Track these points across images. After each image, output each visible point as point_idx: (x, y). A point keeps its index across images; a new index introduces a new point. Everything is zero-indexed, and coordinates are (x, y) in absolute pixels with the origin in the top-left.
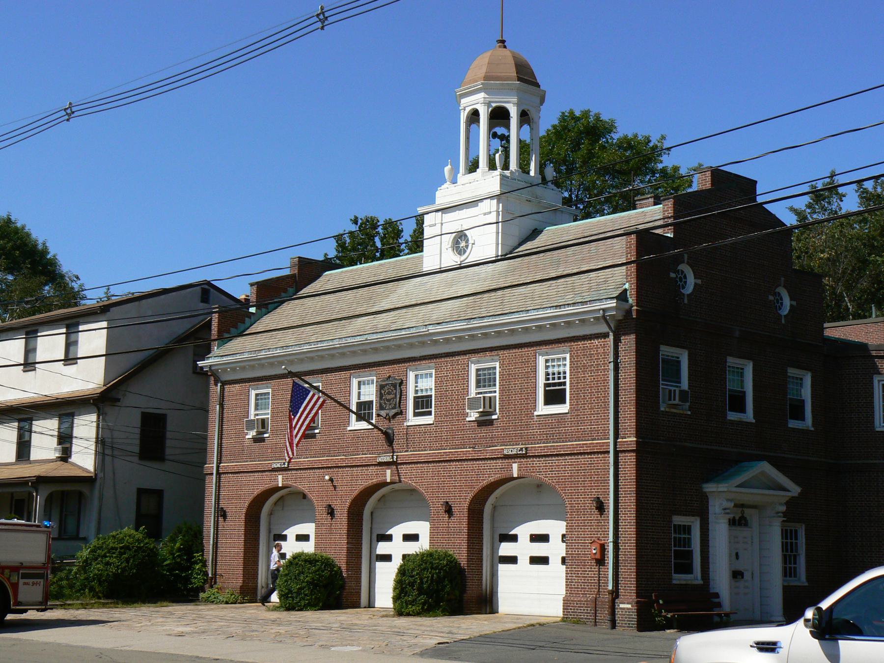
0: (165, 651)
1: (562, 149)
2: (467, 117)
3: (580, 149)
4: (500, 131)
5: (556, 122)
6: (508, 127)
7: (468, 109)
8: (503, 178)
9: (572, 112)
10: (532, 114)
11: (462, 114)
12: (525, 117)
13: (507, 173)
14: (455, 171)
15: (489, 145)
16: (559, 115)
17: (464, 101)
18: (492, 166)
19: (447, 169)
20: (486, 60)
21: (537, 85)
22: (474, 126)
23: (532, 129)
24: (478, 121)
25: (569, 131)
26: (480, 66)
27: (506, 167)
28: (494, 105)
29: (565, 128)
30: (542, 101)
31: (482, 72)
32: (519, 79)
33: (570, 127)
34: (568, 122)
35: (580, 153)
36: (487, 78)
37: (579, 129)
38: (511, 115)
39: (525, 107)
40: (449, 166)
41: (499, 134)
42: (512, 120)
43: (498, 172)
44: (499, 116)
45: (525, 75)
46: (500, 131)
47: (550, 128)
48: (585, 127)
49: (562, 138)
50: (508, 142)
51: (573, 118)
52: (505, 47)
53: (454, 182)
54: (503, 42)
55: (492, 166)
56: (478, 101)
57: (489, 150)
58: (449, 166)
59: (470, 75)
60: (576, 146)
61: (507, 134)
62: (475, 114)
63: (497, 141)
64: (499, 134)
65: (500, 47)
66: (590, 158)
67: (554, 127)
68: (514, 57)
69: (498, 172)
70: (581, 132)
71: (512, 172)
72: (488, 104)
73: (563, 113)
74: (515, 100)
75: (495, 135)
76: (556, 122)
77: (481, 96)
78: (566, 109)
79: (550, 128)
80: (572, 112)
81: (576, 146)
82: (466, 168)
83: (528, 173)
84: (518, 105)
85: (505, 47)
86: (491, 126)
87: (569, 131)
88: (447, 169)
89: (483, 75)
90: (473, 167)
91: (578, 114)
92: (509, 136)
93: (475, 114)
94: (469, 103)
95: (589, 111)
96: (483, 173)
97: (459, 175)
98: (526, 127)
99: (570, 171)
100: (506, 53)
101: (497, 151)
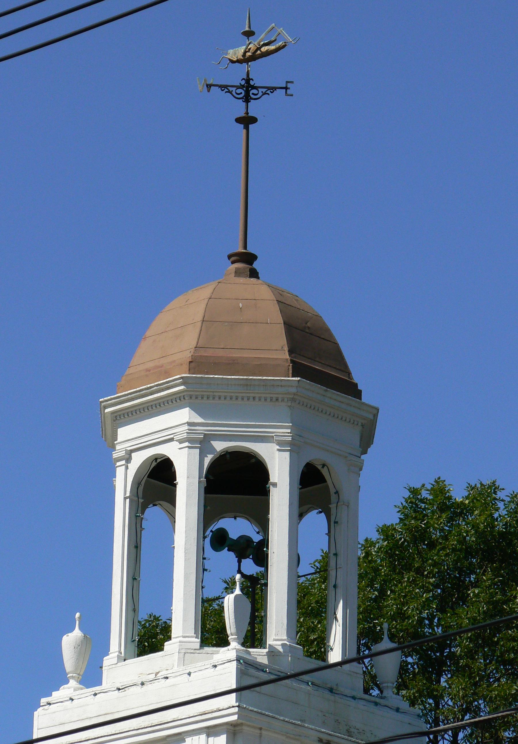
0: (186, 465)
1: (417, 600)
2: (137, 483)
3: (464, 599)
4: (237, 527)
5: (393, 518)
6: (261, 518)
7: (139, 459)
8: (245, 665)
9: (440, 489)
10: (337, 474)
11: (120, 472)
12: (313, 486)
13: (259, 655)
14: (95, 647)
15: (202, 569)
16: (401, 496)
17: (127, 434)
18: (212, 634)
19: (70, 641)
20: (197, 312)
21: (353, 391)
22: (154, 513)
23: (332, 523)
24: (170, 499)
25: (432, 545)
26: (176, 329)
27: (254, 637)
28: (220, 446)
29: (420, 536)
30: (366, 440)
31: (186, 345)
32: (298, 370)
33: (436, 535)
34: (429, 513)
35: (465, 616)
36: (196, 364)
37: (462, 541)
38: (273, 477)
39: (314, 456)
40: (77, 633)
41: (234, 535)
42: (273, 492)
43: (233, 649)
44: (234, 481)
45: (316, 358)
46: (237, 527)
47: (374, 536)
48: (480, 535)
49: (408, 568)
50: (262, 559)
51: (443, 508)
52: (254, 274)
53: (91, 677)
54: (248, 258)
55: (212, 634)
56: (171, 435)
57: (200, 585)
58: (77, 633)
59: (145, 355)
60: (452, 594)
61: (257, 538)
62: (160, 476)
63: (227, 557)
64: (234, 535)
65: (238, 273)
66: (496, 628)
67: (386, 532)
68: (283, 305)
69: (233, 649)
70: (469, 552)
71: (273, 653)
72: (202, 443)
73: (414, 492)
74: (284, 431)
75: (220, 540)
76: (393, 518)
77: (183, 415)
78: (424, 479)
79: (374, 536)
80: (440, 489)
81: (452, 594)
82: (130, 640)
83: (322, 656)
84: (294, 447)
85: (254, 274)
86: (209, 514)
87: (432, 545)
88: (70, 641)
89: (187, 355)
90: (150, 638)
91: (458, 494)
92: (264, 543)
93: (160, 476)
94: (140, 440)
95: (494, 487)
96: (185, 654)
97: (108, 661)
98: (316, 520)
99: (432, 668)
100: (258, 291)
101: (229, 587)
